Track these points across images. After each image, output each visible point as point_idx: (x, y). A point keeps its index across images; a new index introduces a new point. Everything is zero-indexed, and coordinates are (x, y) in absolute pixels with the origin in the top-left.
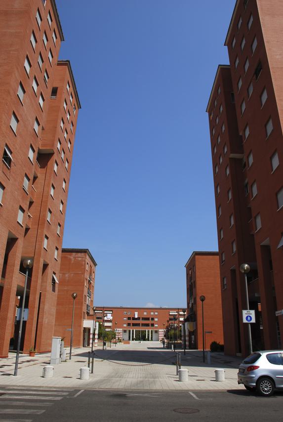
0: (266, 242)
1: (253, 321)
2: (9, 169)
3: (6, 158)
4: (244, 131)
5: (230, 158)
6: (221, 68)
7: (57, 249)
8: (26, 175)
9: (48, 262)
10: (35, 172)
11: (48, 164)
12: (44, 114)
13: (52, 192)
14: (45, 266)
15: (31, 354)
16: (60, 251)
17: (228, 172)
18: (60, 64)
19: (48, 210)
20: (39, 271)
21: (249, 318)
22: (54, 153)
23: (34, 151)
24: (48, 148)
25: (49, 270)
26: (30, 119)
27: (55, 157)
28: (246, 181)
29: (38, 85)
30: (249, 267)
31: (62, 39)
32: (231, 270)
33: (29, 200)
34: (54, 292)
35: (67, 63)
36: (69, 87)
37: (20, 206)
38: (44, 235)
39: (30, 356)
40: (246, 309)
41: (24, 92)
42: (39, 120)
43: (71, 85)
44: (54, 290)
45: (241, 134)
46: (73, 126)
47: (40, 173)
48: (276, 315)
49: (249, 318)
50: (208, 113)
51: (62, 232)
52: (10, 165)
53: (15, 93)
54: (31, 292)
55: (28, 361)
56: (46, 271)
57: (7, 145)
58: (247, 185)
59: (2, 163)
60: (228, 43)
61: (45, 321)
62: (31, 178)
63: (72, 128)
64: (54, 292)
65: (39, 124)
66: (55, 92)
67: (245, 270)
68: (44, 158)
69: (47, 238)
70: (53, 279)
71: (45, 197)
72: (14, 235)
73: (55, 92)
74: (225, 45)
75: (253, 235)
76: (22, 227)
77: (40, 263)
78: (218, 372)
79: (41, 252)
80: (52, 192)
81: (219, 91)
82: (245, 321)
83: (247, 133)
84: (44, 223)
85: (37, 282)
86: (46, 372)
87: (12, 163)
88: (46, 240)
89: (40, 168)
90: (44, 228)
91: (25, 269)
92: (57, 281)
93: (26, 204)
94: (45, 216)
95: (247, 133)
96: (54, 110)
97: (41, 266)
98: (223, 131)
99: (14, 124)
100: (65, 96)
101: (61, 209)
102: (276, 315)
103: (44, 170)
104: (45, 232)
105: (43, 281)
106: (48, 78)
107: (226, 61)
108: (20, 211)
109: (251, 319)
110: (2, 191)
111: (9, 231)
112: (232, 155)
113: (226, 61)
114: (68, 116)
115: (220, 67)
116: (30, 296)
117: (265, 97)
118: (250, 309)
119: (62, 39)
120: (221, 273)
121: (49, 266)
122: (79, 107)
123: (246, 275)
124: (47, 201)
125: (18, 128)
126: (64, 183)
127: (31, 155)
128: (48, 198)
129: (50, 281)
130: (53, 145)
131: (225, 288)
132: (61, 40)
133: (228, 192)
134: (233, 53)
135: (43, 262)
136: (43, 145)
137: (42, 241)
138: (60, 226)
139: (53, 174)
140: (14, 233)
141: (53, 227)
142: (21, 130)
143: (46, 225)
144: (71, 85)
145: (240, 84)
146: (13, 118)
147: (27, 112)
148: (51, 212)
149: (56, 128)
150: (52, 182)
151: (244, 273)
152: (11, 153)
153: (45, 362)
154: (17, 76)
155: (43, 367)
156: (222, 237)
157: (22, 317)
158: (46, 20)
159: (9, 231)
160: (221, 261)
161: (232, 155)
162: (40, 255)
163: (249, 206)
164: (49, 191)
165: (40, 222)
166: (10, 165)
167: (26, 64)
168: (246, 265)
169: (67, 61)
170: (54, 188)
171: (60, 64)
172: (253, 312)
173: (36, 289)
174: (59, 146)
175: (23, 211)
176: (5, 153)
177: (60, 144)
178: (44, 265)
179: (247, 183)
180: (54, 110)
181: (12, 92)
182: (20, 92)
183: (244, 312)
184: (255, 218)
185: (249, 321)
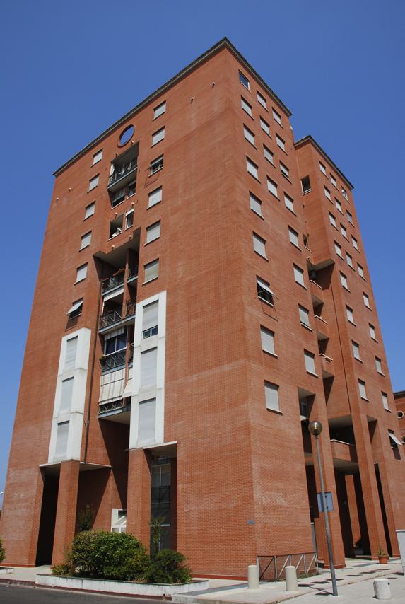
2: (272, 306)
3: (264, 295)
7: (385, 395)
8: (300, 306)
9: (376, 418)
10: (313, 296)
11: (331, 280)
12: (299, 219)
13: (350, 317)
14: (372, 425)
15: (381, 559)
16: (391, 397)
18: (297, 146)
19: (351, 343)
20: (364, 433)
22: (334, 264)
23: (301, 271)
24: (323, 260)
25: (381, 429)
26: (280, 232)
27: (337, 268)
29: (276, 185)
31: (288, 114)
33: (316, 338)
34: (400, 459)
35: (309, 140)
36: (325, 168)
37: (305, 350)
38: (357, 381)
39: (380, 563)
41: (260, 202)
42: (294, 229)
43: (325, 164)
44: (397, 456)
46: (351, 216)
47: (323, 296)
51: (385, 368)
52: (272, 302)
53: (247, 210)
54: (360, 466)
55: (372, 572)
56: (376, 431)
59: (260, 302)
61: (396, 506)
62: (310, 307)
63: (350, 219)
64: (400, 459)
65: (296, 234)
66: (306, 183)
68: (321, 275)
69: (363, 383)
70: (391, 440)
71: (341, 325)
72: (308, 391)
73: (306, 183)
76: (317, 377)
77: (362, 421)
78: (378, 584)
79: (358, 404)
80: (350, 317)
84: (351, 364)
85: (365, 450)
86: (378, 589)
87: (274, 299)
88: (361, 387)
89: (323, 289)
90: (353, 370)
91: (342, 431)
92: (398, 442)
93: (313, 345)
94: (350, 353)
96: (314, 209)
97: (365, 425)
99: (259, 247)
100: (322, 182)
101: (373, 336)
103: (328, 291)
104: (357, 376)
105: (374, 448)
106: (288, 170)
108: (306, 357)
110: (272, 337)
111: (299, 388)
114: (338, 206)
115: (225, 42)
116: (360, 470)
119: (288, 114)
121: (379, 424)
122: (351, 187)
124: (346, 331)
125: (267, 251)
126: (365, 298)
127: (299, 277)
128: (345, 327)
129: (386, 444)
130: (329, 252)
132: (288, 116)
135: (366, 419)
136: (315, 259)
137: (356, 390)
138: (379, 360)
139: (342, 293)
140: (306, 388)
141: (367, 365)
142: (272, 252)
143: (354, 365)
144: (325, 164)
146: (255, 240)
147: (273, 225)
148: (357, 345)
149: (324, 228)
150: (345, 302)
152: (268, 285)
153: (398, 571)
154: (242, 187)
155: (372, 581)
157: (325, 507)
158: (257, 104)
159: (299, 388)
162: (358, 410)
164: (344, 317)
165: (346, 362)
166: (272, 302)
167: (250, 168)
169: (308, 137)
170: (351, 310)
171: (297, 146)
173: (366, 460)
174: (338, 251)
175: (312, 355)
176: (259, 288)
177: (340, 247)
178: (369, 423)
180: (314, 209)
181: (242, 209)
182: (254, 205)
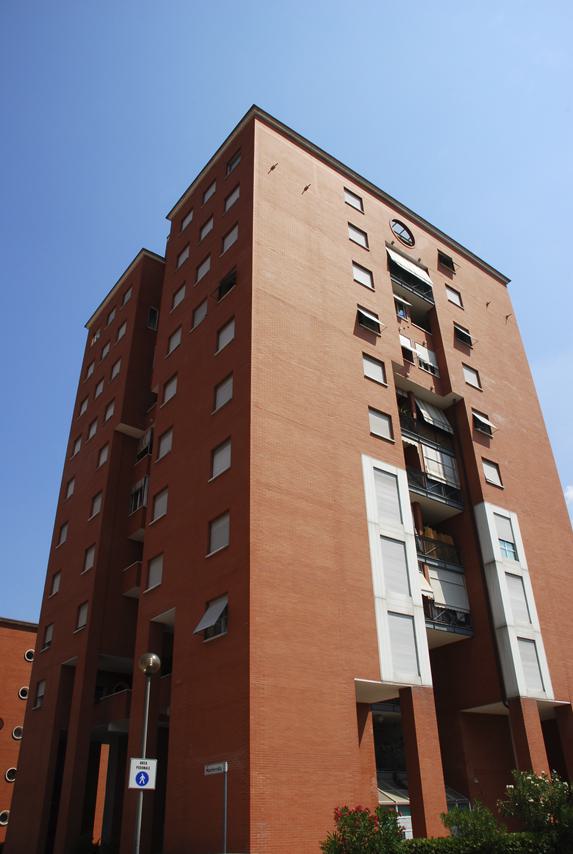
0: (166, 616)
1: (151, 785)
4: (166, 385)
5: (117, 433)
6: (145, 256)
17: (104, 458)
21: (143, 777)
28: (139, 485)
30: (159, 662)
32: (64, 666)
40: (141, 757)
45: (155, 390)
48: (206, 773)
49: (143, 777)
50: (87, 331)
57: (386, 387)
58: (136, 494)
60: (176, 217)
67: (148, 667)
74: (167, 218)
75: (134, 602)
81: (128, 296)
82: (133, 784)
83: (171, 391)
95: (171, 391)
98: (114, 375)
102: (206, 773)
107: (160, 249)
109: (147, 780)
112: (123, 427)
113: (160, 249)
117: (227, 336)
118: (147, 757)
120: (33, 671)
123: (149, 679)
131: (38, 706)
133: (94, 499)
134: (175, 241)
145: (180, 297)
151: (147, 674)
152: (486, 417)
156: (56, 590)
160: (41, 643)
161: (123, 427)
163: (134, 536)
168: (154, 657)
172: (152, 764)
179: (141, 490)
183: (135, 763)
184: (150, 562)
185: (142, 784)
